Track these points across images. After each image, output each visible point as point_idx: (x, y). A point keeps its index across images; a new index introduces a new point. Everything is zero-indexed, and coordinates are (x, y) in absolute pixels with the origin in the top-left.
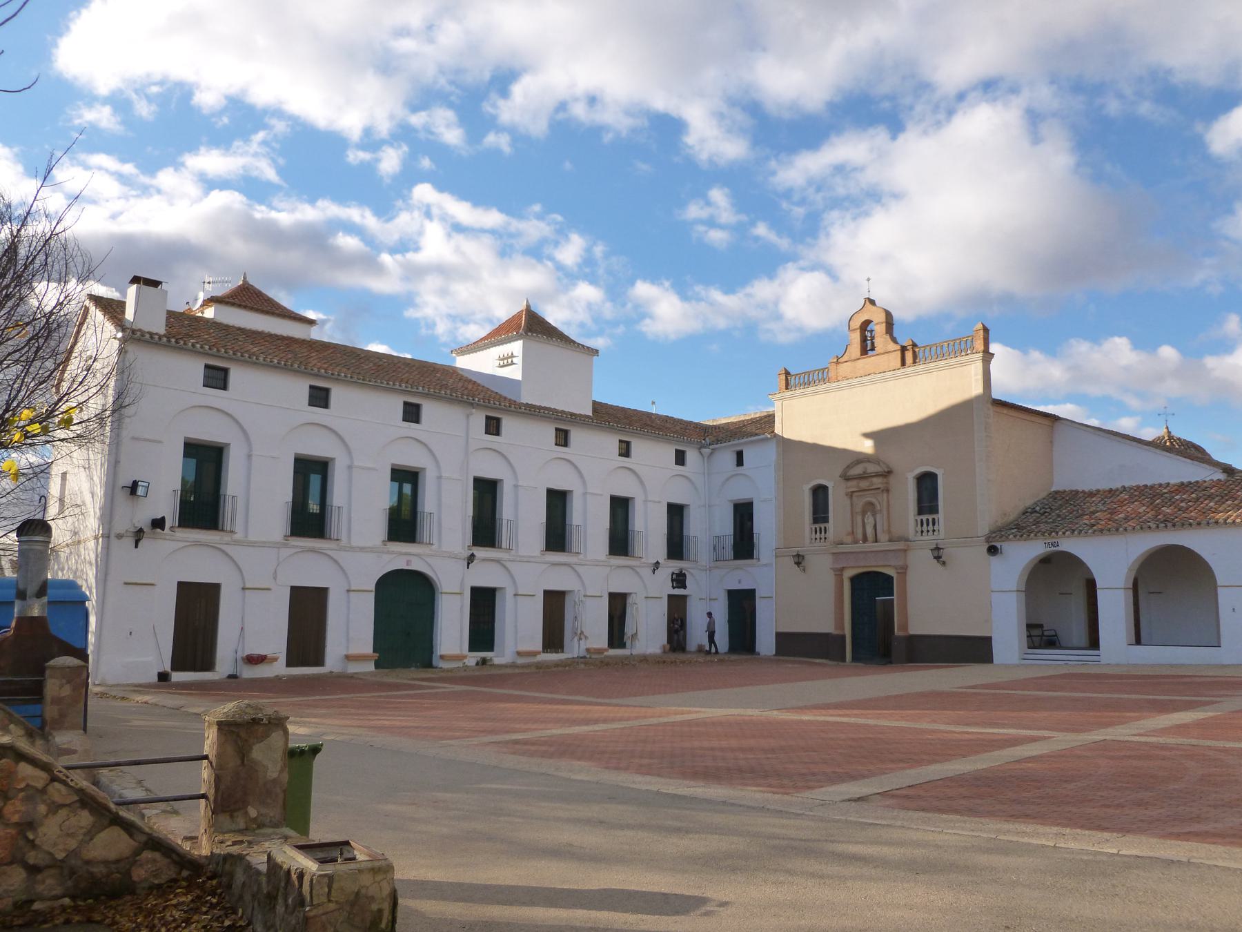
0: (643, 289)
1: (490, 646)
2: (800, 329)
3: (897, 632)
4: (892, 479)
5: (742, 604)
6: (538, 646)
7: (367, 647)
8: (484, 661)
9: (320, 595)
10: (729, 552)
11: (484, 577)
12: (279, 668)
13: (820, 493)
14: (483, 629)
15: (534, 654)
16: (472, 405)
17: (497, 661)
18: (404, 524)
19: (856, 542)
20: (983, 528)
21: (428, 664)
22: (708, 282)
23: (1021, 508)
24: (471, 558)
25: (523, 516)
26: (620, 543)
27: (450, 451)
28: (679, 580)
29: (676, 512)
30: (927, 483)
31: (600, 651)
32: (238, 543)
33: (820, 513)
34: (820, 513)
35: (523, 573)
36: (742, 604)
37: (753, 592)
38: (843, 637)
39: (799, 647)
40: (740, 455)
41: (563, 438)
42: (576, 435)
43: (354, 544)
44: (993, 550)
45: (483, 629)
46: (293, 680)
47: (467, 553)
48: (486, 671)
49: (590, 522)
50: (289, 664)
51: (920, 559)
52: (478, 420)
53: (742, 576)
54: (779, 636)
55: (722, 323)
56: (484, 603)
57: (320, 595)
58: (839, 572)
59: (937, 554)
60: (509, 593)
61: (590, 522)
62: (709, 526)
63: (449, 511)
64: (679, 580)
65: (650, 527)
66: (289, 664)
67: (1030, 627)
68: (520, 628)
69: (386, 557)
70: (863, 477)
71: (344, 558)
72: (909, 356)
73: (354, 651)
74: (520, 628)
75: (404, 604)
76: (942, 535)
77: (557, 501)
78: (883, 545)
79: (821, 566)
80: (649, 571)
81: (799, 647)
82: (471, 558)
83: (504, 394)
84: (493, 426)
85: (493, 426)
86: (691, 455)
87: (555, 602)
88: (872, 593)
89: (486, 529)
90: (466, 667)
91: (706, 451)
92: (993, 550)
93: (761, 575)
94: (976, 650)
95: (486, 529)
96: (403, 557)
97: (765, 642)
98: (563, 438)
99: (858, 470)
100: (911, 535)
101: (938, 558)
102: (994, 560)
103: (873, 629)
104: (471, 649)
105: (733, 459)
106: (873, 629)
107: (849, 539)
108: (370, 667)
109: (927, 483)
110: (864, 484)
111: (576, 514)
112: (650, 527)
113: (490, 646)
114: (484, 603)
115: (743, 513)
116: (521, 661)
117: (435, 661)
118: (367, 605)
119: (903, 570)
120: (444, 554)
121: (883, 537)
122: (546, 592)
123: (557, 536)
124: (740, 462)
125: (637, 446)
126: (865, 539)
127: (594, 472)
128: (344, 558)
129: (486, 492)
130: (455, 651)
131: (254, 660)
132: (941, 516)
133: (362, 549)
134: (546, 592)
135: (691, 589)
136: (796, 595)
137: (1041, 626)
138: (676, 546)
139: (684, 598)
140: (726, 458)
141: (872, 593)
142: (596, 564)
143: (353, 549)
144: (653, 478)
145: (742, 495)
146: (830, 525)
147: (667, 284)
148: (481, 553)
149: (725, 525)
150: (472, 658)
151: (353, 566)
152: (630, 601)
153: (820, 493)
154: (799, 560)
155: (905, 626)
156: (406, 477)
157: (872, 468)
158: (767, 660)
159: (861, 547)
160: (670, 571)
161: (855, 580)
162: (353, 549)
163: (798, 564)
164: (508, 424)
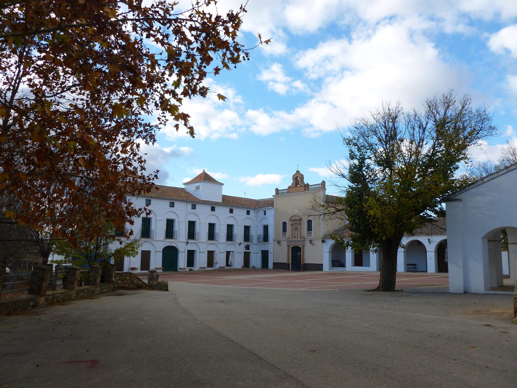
0: (251, 113)
1: (193, 266)
2: (320, 131)
3: (302, 263)
4: (301, 221)
5: (265, 254)
6: (206, 265)
7: (161, 266)
8: (191, 270)
9: (149, 252)
10: (262, 240)
11: (191, 247)
12: (139, 271)
13: (284, 224)
14: (191, 262)
15: (205, 268)
16: (188, 202)
17: (194, 270)
18: (170, 233)
19: (292, 238)
20: (322, 236)
21: (176, 270)
22: (279, 109)
23: (335, 229)
24: (187, 243)
25: (202, 230)
26: (230, 237)
27: (182, 214)
28: (247, 247)
29: (247, 229)
30: (309, 222)
31: (223, 267)
32: (155, 241)
33: (285, 230)
34: (285, 230)
35: (202, 246)
36: (265, 254)
37: (268, 251)
38: (289, 264)
39: (279, 267)
40: (265, 212)
41: (213, 209)
42: (217, 208)
43: (158, 239)
44: (323, 241)
45: (191, 262)
46: (142, 273)
47: (186, 241)
48: (192, 272)
49: (221, 232)
50: (141, 270)
51: (307, 243)
52: (190, 206)
53: (265, 247)
54: (274, 263)
55: (287, 127)
56: (191, 254)
57: (149, 252)
58: (289, 246)
59: (311, 242)
60: (198, 251)
61: (221, 232)
62: (256, 232)
63: (181, 230)
64: (247, 247)
65: (239, 233)
66: (141, 270)
67: (332, 261)
68: (201, 260)
69: (165, 243)
70: (295, 220)
71: (155, 243)
72: (307, 188)
73: (157, 267)
74: (201, 260)
75: (170, 255)
76: (312, 237)
77: (212, 226)
78: (299, 239)
79: (284, 244)
80: (238, 245)
81: (279, 267)
82: (187, 243)
83: (197, 197)
84: (194, 207)
85: (194, 207)
86: (252, 212)
87: (211, 254)
88: (296, 252)
89: (191, 235)
90: (186, 271)
91: (256, 210)
92: (323, 241)
93: (270, 247)
94: (319, 267)
95: (191, 235)
96: (169, 242)
97: (271, 265)
98: (213, 209)
99: (293, 218)
100: (306, 236)
101: (311, 243)
102: (324, 244)
103: (296, 262)
104: (187, 266)
105: (263, 213)
106: (296, 262)
107: (291, 237)
108: (161, 271)
109: (309, 222)
110: (295, 222)
111: (217, 230)
112: (239, 233)
113: (193, 266)
114: (191, 254)
115: (266, 228)
116: (201, 270)
117: (178, 270)
118: (160, 256)
119: (304, 246)
120: (181, 241)
121: (299, 237)
122: (208, 251)
123: (211, 236)
124: (265, 214)
125: (235, 210)
126: (295, 237)
127: (222, 218)
128: (155, 243)
129: (192, 225)
130: (183, 267)
131: (133, 269)
132: (312, 232)
133: (159, 241)
134: (208, 251)
135: (251, 250)
136: (280, 254)
137: (339, 261)
138: (247, 237)
139: (249, 252)
140: (261, 213)
141: (296, 252)
142: (223, 243)
143: (157, 241)
144: (240, 219)
145: (265, 223)
146: (287, 233)
147: (261, 110)
148: (190, 241)
149: (261, 232)
150: (188, 269)
151: (156, 245)
152: (215, 253)
153: (284, 224)
154: (279, 242)
155: (304, 261)
156: (415, 346)
157: (297, 218)
158: (271, 270)
159: (293, 239)
160: (244, 245)
161: (292, 248)
162: (157, 241)
163: (278, 243)
164: (198, 206)
